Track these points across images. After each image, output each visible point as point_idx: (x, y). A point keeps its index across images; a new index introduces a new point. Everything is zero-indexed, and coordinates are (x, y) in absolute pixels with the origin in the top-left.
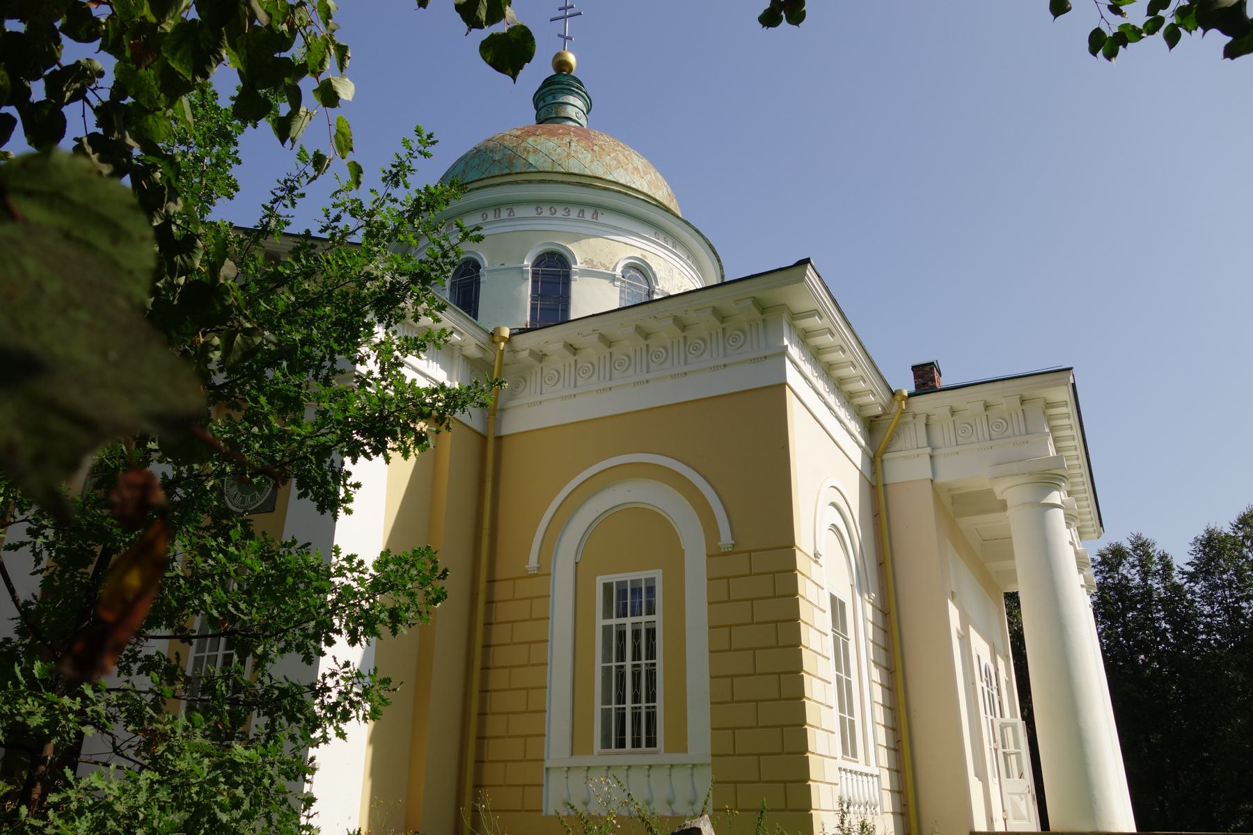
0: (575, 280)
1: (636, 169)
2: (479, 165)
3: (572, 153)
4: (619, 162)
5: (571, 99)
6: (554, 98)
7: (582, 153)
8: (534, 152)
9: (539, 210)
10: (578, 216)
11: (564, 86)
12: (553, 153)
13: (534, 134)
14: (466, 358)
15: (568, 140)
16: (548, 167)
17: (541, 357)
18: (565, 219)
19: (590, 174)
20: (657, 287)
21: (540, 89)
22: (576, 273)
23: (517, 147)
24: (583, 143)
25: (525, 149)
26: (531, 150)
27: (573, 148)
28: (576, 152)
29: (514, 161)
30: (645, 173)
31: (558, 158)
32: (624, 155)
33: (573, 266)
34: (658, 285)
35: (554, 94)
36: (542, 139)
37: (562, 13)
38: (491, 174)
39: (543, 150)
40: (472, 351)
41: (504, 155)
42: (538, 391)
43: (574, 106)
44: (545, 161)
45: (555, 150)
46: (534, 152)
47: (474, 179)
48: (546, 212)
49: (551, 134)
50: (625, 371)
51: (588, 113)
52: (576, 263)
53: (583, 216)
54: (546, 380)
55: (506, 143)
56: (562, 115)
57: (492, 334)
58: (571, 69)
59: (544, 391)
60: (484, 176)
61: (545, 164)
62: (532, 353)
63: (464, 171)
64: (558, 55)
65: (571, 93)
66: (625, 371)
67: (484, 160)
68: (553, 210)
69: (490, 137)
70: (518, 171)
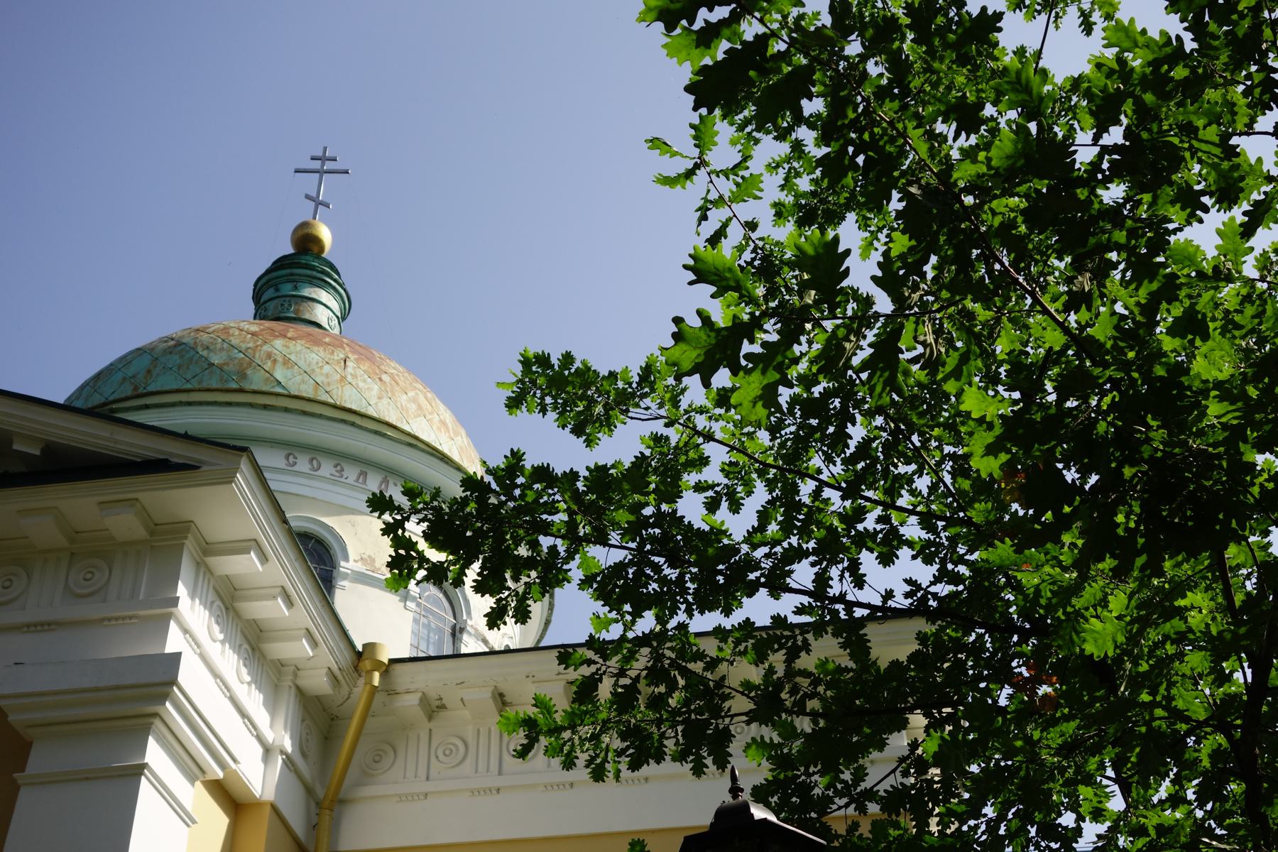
0: (343, 588)
1: (443, 423)
2: (180, 367)
3: (349, 378)
4: (420, 407)
5: (323, 296)
6: (296, 288)
7: (365, 381)
8: (284, 364)
9: (291, 459)
10: (357, 480)
11: (315, 273)
12: (317, 370)
13: (285, 336)
14: (300, 692)
15: (342, 356)
16: (307, 391)
17: (433, 708)
18: (335, 482)
19: (375, 415)
20: (469, 622)
21: (268, 272)
22: (345, 576)
23: (255, 349)
24: (366, 366)
25: (269, 355)
26: (280, 360)
27: (350, 370)
28: (355, 376)
29: (249, 372)
30: (456, 434)
31: (326, 381)
32: (426, 398)
33: (343, 563)
34: (471, 619)
35: (296, 282)
36: (299, 346)
37: (316, 165)
38: (205, 385)
39: (301, 363)
40: (318, 682)
41: (232, 359)
42: (422, 772)
43: (324, 305)
44: (303, 381)
45: (321, 368)
46: (284, 364)
47: (167, 388)
48: (303, 464)
49: (311, 341)
50: (454, 767)
51: (344, 318)
52: (346, 559)
53: (365, 482)
54: (440, 753)
55: (234, 341)
56: (307, 316)
57: (359, 655)
58: (322, 249)
59: (433, 774)
60: (189, 386)
61: (303, 387)
62: (424, 700)
63: (149, 372)
64: (305, 225)
65: (324, 285)
66: (454, 767)
67: (191, 359)
68: (315, 463)
69: (197, 325)
70: (255, 387)
